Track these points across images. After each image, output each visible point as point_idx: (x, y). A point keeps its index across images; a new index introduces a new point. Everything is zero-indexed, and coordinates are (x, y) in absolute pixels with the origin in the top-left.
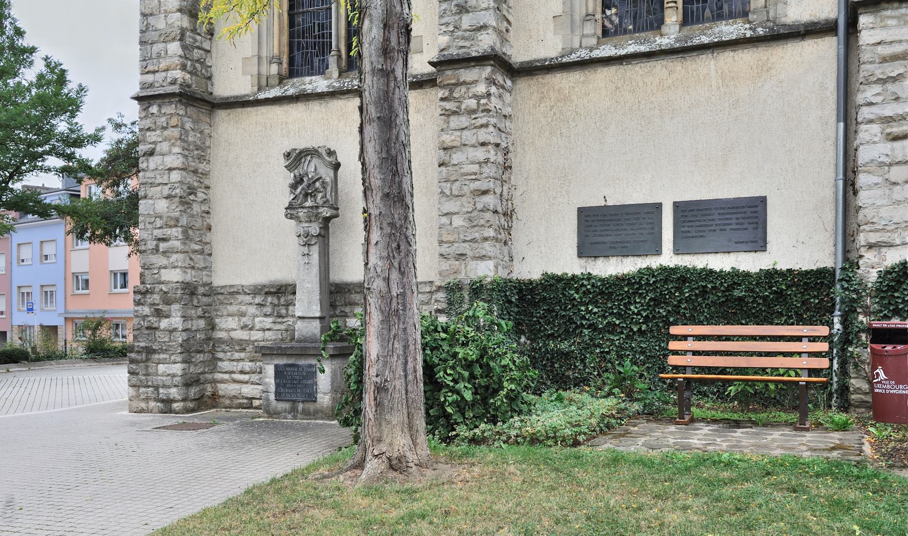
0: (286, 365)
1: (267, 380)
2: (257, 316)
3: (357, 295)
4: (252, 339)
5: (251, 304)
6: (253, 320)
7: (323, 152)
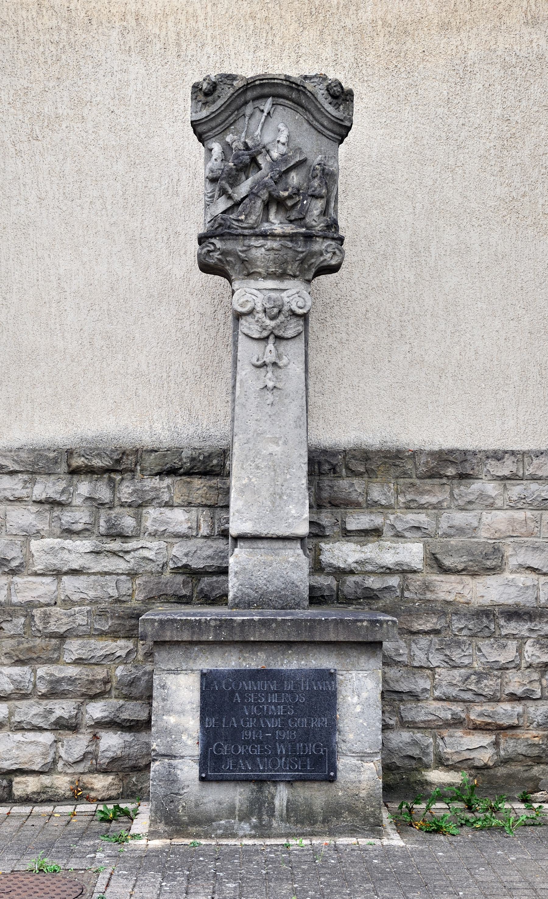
0: (239, 675)
1: (172, 720)
2: (38, 535)
3: (355, 481)
4: (15, 599)
5: (19, 500)
6: (26, 544)
7: (321, 93)
